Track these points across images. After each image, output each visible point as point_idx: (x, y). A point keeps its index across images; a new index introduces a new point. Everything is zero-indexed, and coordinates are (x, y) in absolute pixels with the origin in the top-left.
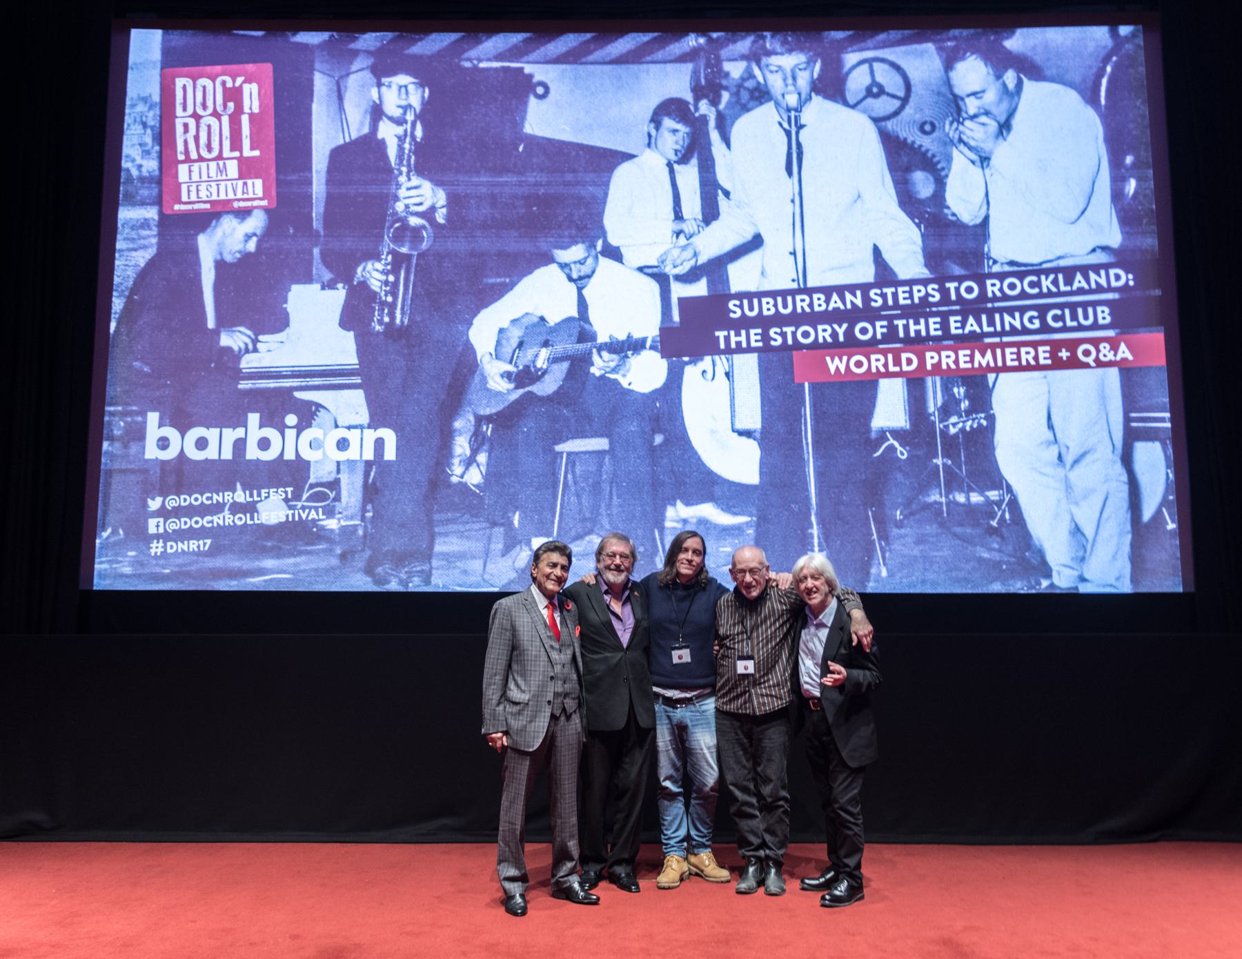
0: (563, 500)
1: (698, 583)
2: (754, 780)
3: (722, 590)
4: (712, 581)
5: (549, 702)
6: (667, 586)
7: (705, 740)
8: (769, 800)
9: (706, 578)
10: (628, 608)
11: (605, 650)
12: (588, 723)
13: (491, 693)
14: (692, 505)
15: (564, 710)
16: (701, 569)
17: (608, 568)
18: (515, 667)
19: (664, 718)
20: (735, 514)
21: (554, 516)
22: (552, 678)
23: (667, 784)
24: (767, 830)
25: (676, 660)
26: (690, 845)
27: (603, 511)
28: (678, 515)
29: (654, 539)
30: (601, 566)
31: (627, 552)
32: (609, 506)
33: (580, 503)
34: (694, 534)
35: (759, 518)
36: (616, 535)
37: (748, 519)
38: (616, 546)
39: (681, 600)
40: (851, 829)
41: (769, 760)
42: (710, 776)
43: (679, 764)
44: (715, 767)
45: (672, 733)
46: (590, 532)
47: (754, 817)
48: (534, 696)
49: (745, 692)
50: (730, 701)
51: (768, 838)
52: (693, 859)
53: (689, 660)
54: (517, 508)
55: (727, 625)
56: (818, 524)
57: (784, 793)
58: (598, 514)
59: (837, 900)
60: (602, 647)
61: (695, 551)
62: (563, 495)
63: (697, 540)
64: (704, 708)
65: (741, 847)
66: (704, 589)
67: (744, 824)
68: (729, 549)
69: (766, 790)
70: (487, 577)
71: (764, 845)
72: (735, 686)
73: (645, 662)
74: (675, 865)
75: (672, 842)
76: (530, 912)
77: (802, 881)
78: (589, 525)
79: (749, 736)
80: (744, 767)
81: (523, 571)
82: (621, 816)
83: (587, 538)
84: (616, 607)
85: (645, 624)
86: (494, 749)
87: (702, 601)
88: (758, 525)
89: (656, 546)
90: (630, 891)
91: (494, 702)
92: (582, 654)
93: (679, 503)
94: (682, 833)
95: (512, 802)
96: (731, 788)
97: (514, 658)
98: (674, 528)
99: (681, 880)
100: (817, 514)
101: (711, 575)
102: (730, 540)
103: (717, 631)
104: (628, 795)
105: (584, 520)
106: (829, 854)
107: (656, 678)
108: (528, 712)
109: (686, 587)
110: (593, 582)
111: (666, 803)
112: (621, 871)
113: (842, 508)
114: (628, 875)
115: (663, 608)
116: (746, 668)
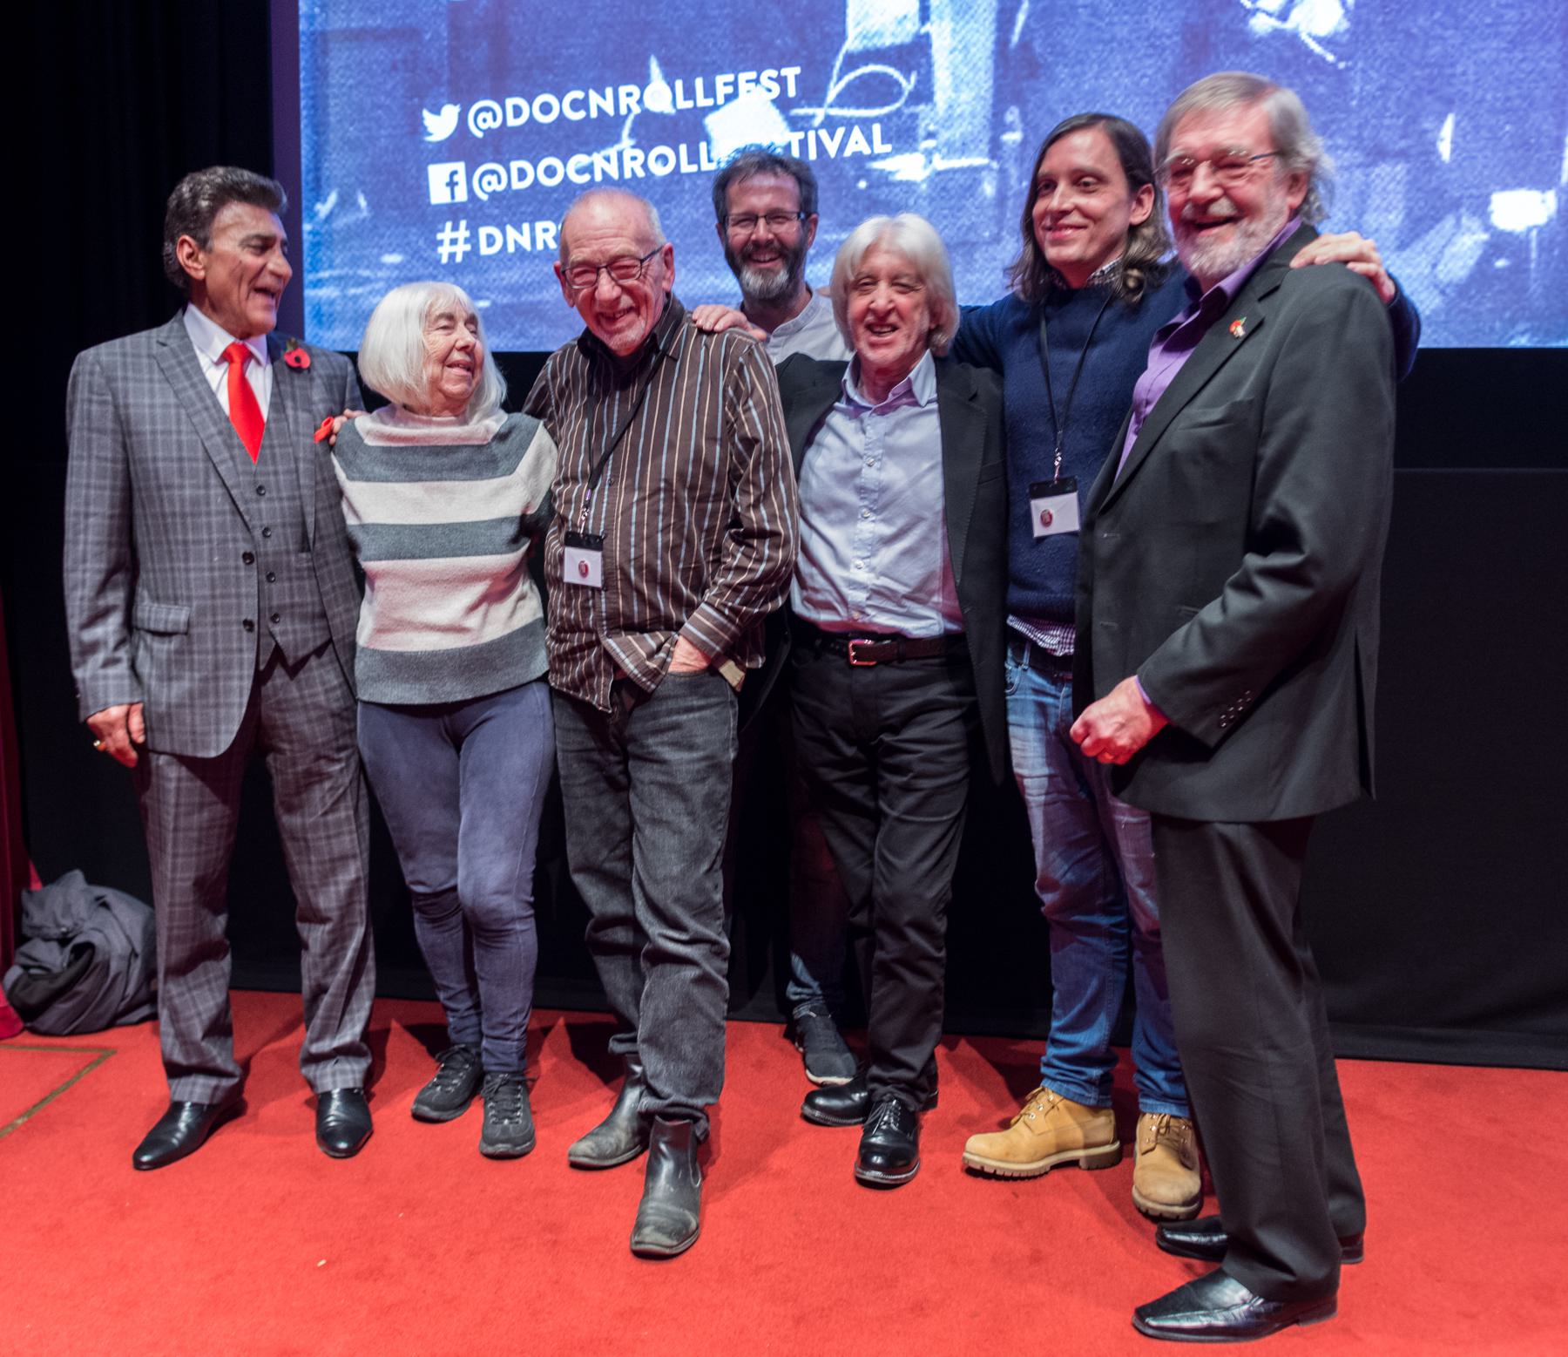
5: (248, 624)
48: (201, 611)
54: (1449, 104)
86: (111, 760)
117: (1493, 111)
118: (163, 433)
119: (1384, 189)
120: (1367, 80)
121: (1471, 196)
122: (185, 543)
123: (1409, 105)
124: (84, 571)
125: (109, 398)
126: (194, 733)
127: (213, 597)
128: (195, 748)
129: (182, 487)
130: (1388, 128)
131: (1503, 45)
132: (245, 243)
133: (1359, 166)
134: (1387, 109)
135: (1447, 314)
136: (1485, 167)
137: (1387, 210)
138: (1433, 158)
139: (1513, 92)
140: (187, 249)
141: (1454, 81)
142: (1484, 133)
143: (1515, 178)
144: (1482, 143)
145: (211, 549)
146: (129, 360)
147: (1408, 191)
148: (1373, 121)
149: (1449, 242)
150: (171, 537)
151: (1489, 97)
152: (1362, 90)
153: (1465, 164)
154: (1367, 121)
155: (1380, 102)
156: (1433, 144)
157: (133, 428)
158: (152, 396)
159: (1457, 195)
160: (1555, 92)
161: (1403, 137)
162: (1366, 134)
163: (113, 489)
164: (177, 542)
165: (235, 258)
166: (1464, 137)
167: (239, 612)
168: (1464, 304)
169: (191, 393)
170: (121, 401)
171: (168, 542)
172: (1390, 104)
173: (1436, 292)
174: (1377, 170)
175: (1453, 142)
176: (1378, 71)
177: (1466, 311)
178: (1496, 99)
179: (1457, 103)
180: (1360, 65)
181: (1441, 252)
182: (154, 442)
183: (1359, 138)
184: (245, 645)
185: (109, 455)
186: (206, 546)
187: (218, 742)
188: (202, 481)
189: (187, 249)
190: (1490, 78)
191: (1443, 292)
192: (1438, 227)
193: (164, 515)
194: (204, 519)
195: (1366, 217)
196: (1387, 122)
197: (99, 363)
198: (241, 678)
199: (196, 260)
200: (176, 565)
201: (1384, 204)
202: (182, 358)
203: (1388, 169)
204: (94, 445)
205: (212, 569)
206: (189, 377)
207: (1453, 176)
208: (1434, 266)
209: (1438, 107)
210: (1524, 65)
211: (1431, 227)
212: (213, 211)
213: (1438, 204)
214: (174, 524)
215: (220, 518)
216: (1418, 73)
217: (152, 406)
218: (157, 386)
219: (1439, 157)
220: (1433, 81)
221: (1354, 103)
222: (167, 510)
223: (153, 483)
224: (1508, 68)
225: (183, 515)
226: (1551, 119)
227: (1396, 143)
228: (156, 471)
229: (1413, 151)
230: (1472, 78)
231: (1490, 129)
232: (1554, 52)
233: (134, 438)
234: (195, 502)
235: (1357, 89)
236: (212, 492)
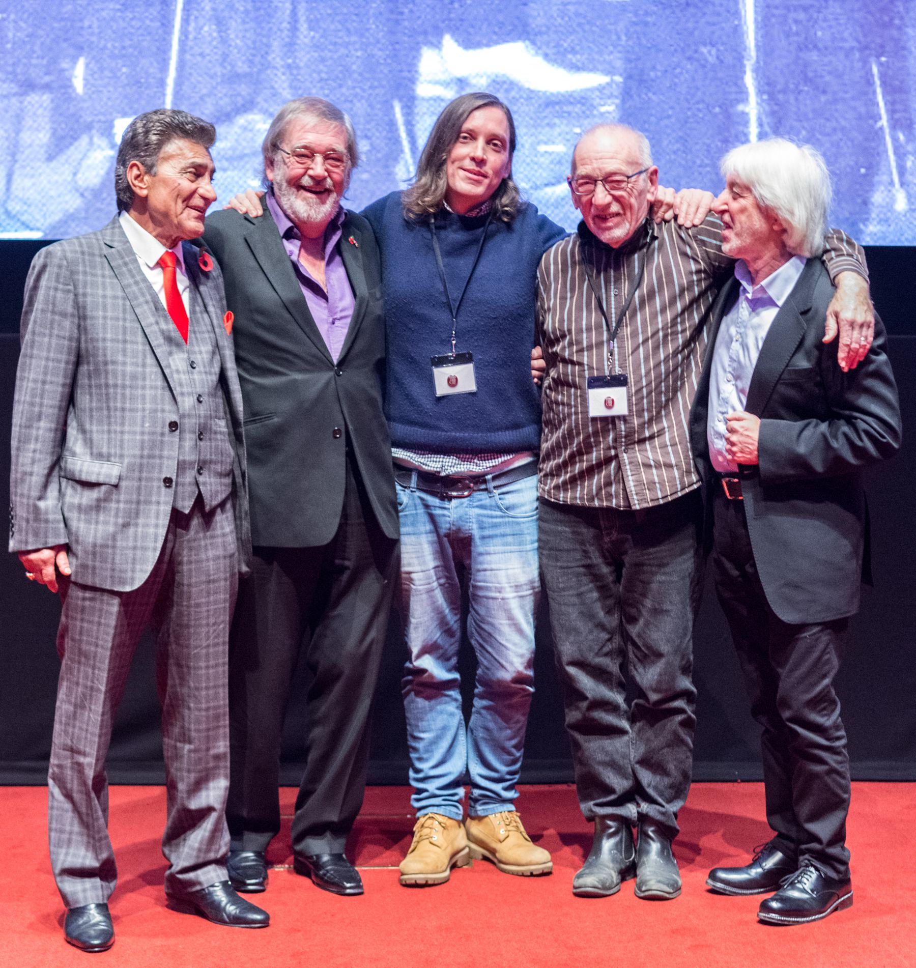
0: (184, 33)
1: (494, 214)
2: (622, 653)
3: (550, 233)
4: (524, 210)
5: (168, 482)
6: (423, 220)
7: (510, 572)
8: (654, 697)
9: (513, 202)
10: (339, 272)
11: (289, 364)
12: (254, 529)
13: (29, 458)
14: (478, 45)
15: (199, 501)
16: (503, 185)
17: (295, 184)
18: (83, 399)
19: (424, 518)
20: (576, 68)
21: (164, 68)
22: (173, 426)
23: (427, 663)
24: (645, 762)
25: (442, 389)
26: (469, 798)
27: (276, 57)
28: (446, 68)
29: (392, 124)
30: (278, 175)
31: (341, 148)
32: (290, 46)
33: (224, 41)
34: (491, 102)
35: (629, 77)
36: (312, 104)
37: (603, 79)
38: (311, 131)
39: (455, 251)
40: (822, 761)
41: (657, 612)
42: (513, 650)
43: (452, 619)
44: (529, 631)
45: (441, 552)
46: (247, 106)
47: (621, 732)
48: (131, 468)
49: (608, 460)
50: (573, 481)
51: (646, 777)
52: (476, 829)
53: (472, 387)
54: (80, 49)
55: (565, 307)
56: (760, 92)
57: (685, 683)
58: (266, 66)
59: (795, 910)
60: (285, 359)
61: (491, 140)
62: (186, 21)
63: (495, 113)
64: (509, 499)
65: (587, 798)
66: (509, 227)
67: (596, 748)
68: (560, 148)
69: (648, 676)
70: (14, 207)
71: (637, 792)
72: (585, 449)
73: (376, 394)
74: (437, 836)
75: (431, 787)
76: (121, 941)
77: (713, 876)
78: (244, 89)
79: (615, 560)
80: (601, 626)
81: (97, 193)
82: (319, 733)
83: (241, 120)
84: (314, 269)
85: (377, 309)
86: (39, 586)
87: (500, 259)
88: (626, 94)
89: (397, 141)
90: (341, 892)
91: (36, 480)
92: (241, 379)
93: (448, 41)
94: (454, 768)
95: (80, 706)
96: (572, 670)
97: (83, 381)
98: (438, 99)
99: (454, 866)
100: (756, 70)
101: (523, 198)
102: (562, 126)
103: (539, 325)
104: (338, 688)
105: (234, 78)
106: (770, 813)
107: (401, 430)
108: (119, 504)
109: (467, 223)
110: (256, 210)
111: (421, 702)
112: (321, 848)
113: (814, 56)
114: (337, 858)
115: (418, 268)
116: (609, 404)
117: (113, 57)
118: (112, 319)
119: (34, 114)
120: (18, 29)
121: (99, 121)
122: (123, 409)
123: (50, 49)
124: (38, 428)
125: (71, 287)
126: (113, 570)
127: (142, 457)
128: (113, 583)
129: (124, 364)
130: (35, 66)
131: (118, 7)
132: (184, 171)
133: (15, 94)
134: (34, 52)
135: (87, 211)
136: (109, 99)
137: (37, 130)
138: (70, 91)
139: (127, 43)
140: (135, 172)
141: (84, 33)
142: (107, 73)
143: (131, 108)
144: (106, 80)
145: (144, 417)
146: (87, 257)
147: (53, 116)
148: (24, 61)
149: (85, 156)
150: (112, 404)
151: (109, 45)
152: (14, 36)
153: (94, 96)
154: (19, 61)
155: (28, 47)
156: (70, 80)
157: (89, 313)
158: (104, 288)
159: (89, 119)
160: (157, 44)
161: (46, 74)
162: (19, 70)
163: (67, 363)
164: (116, 409)
165: (174, 181)
166: (92, 75)
167: (161, 471)
168: (98, 205)
169: (135, 288)
170: (81, 291)
171: (108, 409)
172: (36, 48)
173: (77, 195)
174: (28, 99)
175: (85, 79)
176: (25, 22)
177: (100, 210)
178: (114, 47)
179: (86, 49)
180: (12, 16)
181: (79, 164)
182: (104, 325)
183: (14, 73)
184: (162, 499)
185: (67, 334)
186: (139, 414)
187: (133, 579)
188: (140, 360)
189: (135, 172)
190: (109, 31)
191: (82, 195)
192: (76, 144)
193: (107, 386)
194: (140, 392)
195: (22, 135)
196: (34, 61)
197: (65, 258)
198: (156, 526)
199: (142, 181)
200: (113, 428)
201: (35, 125)
202: (127, 259)
203: (37, 98)
204: (56, 326)
205: (143, 433)
206: (133, 276)
207: (85, 105)
208: (75, 174)
209: (72, 51)
210: (133, 23)
211: (71, 144)
212: (160, 144)
213: (76, 126)
214: (116, 393)
215: (153, 392)
216: (56, 25)
217: (104, 296)
218: (108, 280)
219: (74, 90)
220: (67, 32)
221: (9, 46)
222: (111, 382)
223: (100, 359)
224: (122, 24)
225: (124, 387)
226: (155, 64)
227: (41, 78)
228: (105, 349)
229: (55, 85)
230: (96, 31)
231: (112, 71)
232: (155, 13)
233: (89, 322)
234: (134, 377)
235: (10, 35)
236: (148, 370)
